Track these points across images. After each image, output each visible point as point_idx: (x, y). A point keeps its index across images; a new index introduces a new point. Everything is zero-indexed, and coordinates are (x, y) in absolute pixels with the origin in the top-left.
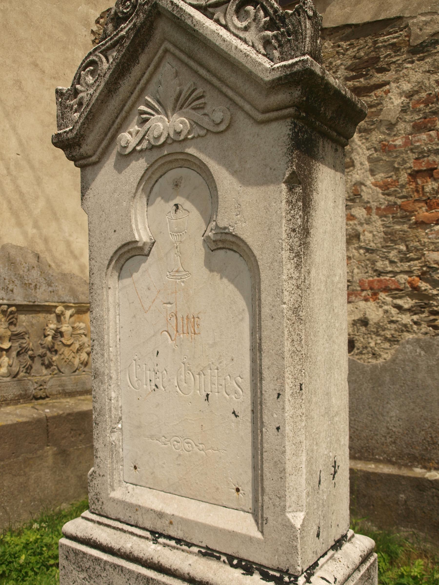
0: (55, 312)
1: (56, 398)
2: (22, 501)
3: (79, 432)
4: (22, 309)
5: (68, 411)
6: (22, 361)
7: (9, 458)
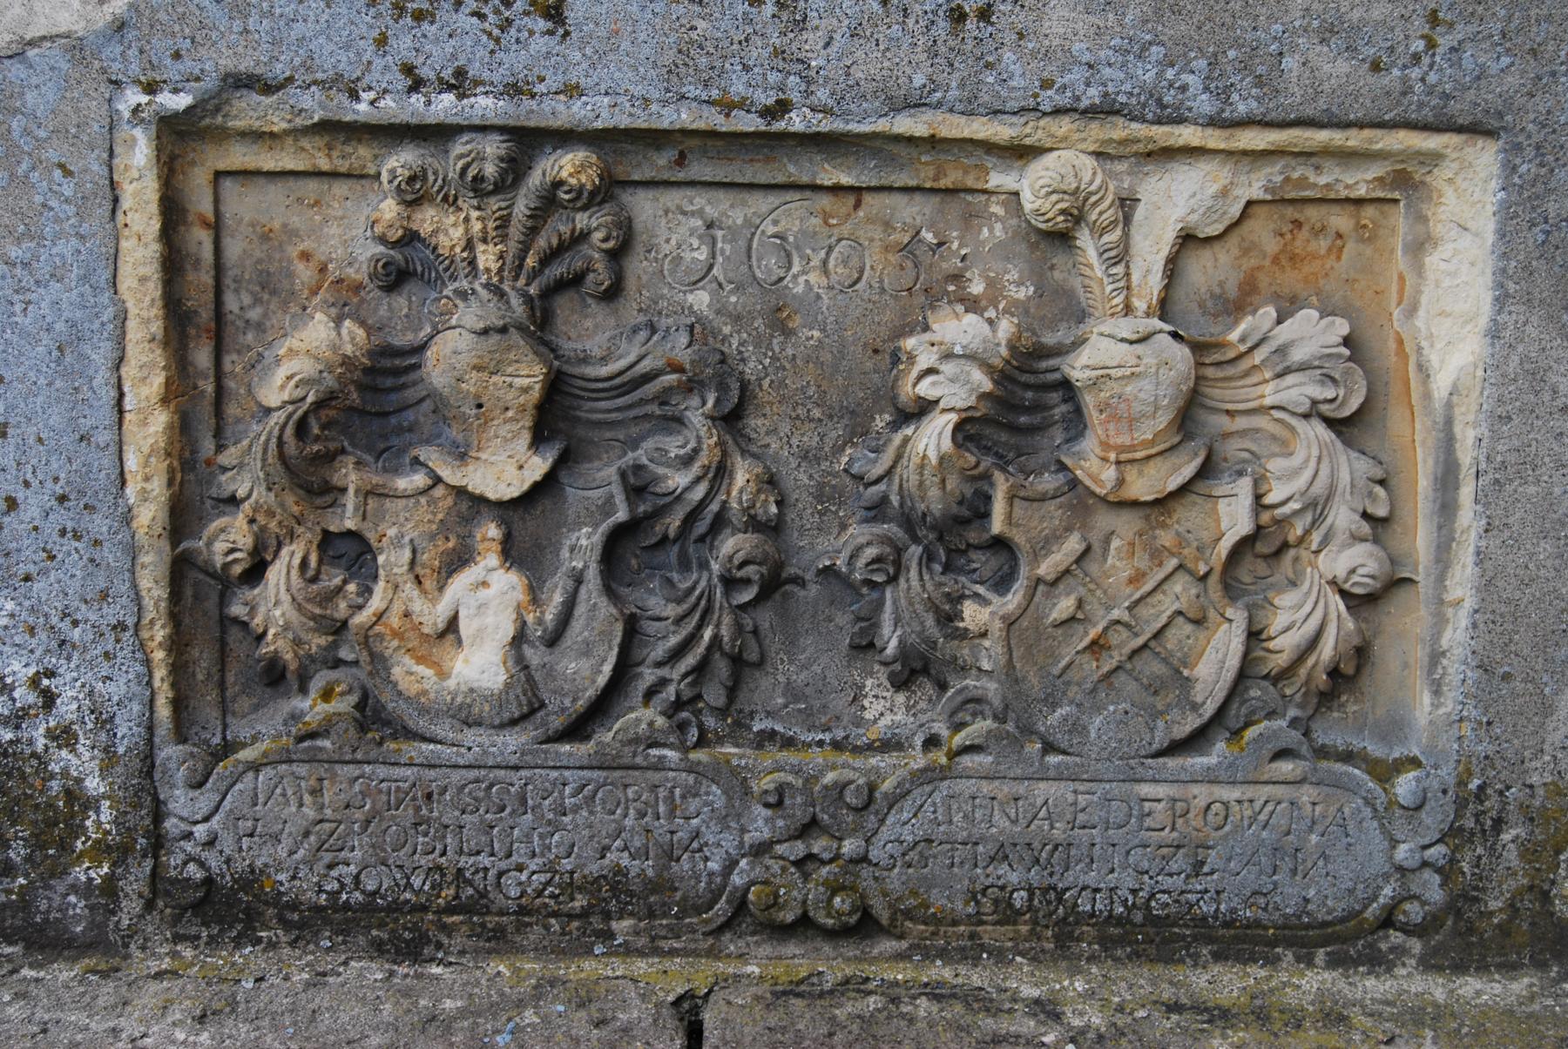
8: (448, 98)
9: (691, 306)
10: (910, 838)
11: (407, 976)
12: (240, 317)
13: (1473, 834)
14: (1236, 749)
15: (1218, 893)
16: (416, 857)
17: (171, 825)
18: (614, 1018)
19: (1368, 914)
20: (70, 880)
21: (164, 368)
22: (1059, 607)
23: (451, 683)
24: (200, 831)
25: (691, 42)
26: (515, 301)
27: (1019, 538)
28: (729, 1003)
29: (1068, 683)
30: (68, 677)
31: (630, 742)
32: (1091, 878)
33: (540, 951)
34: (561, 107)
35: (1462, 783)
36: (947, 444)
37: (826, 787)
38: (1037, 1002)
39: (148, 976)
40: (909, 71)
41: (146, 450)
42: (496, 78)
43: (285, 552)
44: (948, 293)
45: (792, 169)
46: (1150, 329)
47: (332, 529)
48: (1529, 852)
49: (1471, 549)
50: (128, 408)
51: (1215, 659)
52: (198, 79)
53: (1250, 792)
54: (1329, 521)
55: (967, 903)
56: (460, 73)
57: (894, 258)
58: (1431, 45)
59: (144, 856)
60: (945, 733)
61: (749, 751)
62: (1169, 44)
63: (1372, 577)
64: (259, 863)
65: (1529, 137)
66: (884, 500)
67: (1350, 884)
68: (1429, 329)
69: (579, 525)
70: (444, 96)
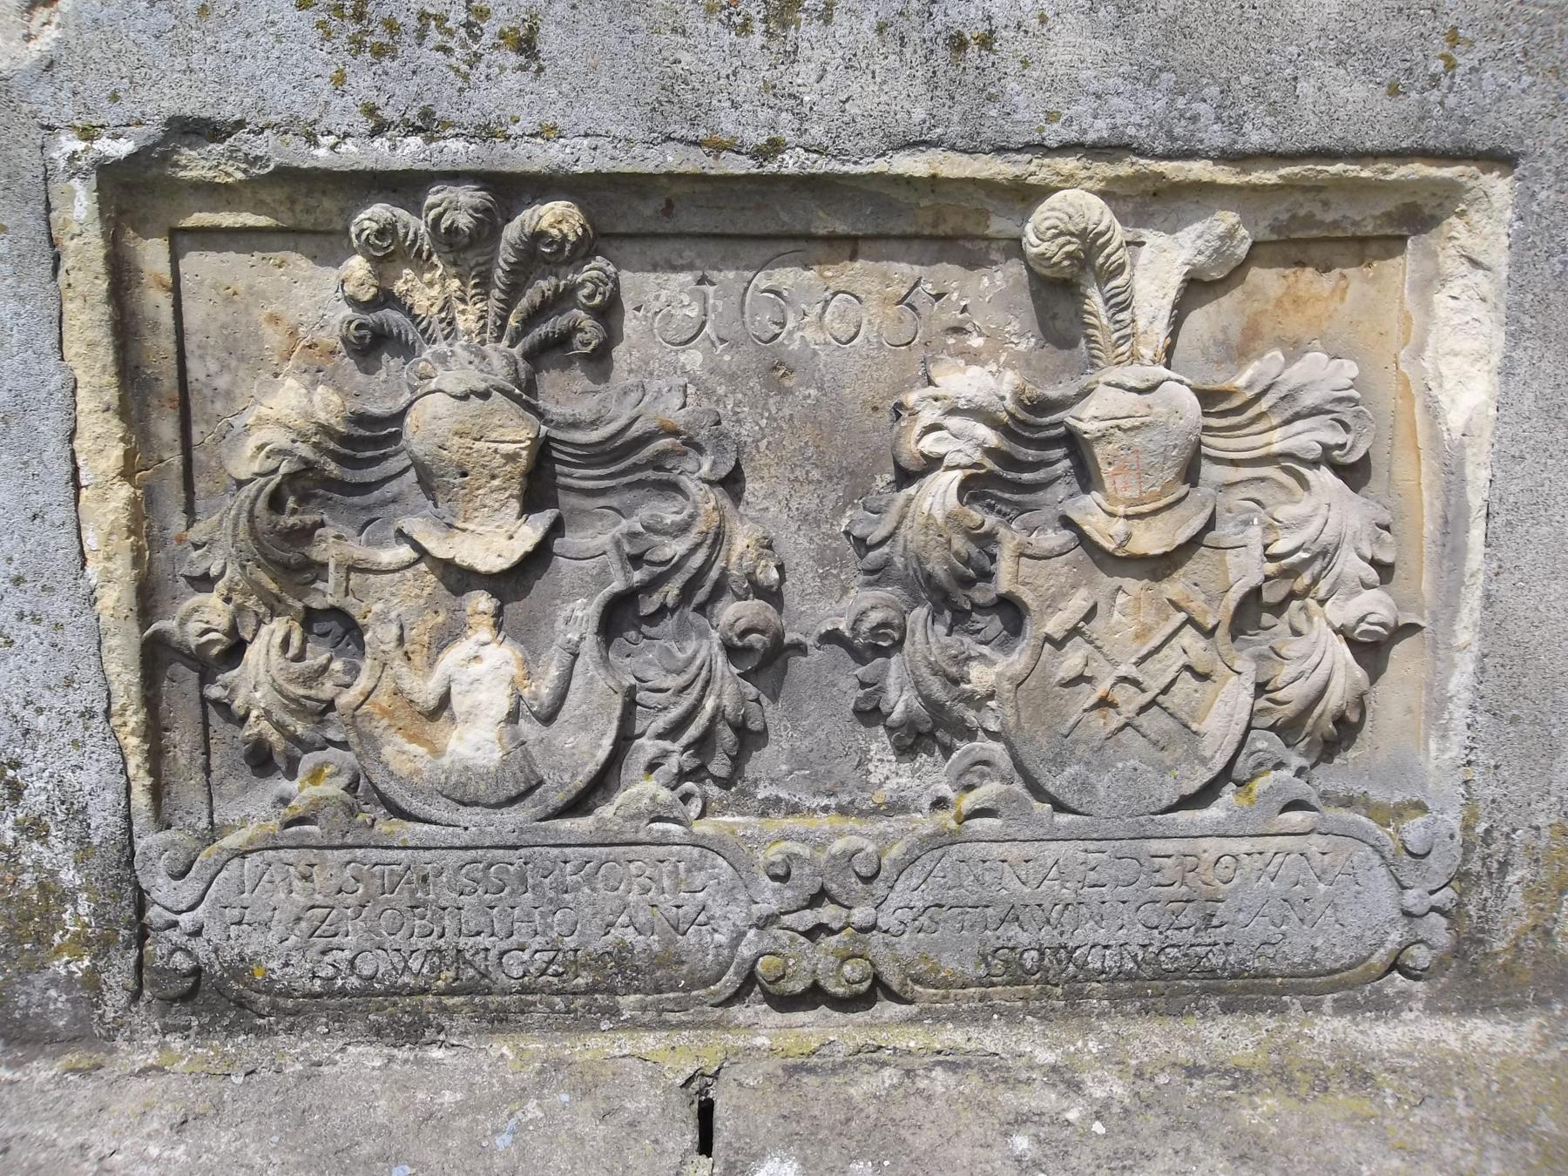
0: (1015, 247)
4: (636, 213)
8: (415, 142)
9: (683, 366)
10: (920, 904)
11: (406, 1061)
12: (207, 386)
13: (1479, 877)
14: (1246, 803)
15: (1227, 944)
16: (413, 940)
17: (154, 914)
18: (622, 1108)
19: (1374, 960)
20: (49, 974)
21: (122, 439)
22: (1065, 665)
23: (446, 761)
24: (185, 920)
25: (675, 77)
26: (497, 362)
27: (1027, 596)
28: (740, 1084)
29: (1076, 742)
30: (35, 767)
31: (632, 817)
32: (1101, 935)
33: (545, 1028)
34: (538, 151)
35: (1467, 827)
36: (952, 500)
37: (834, 857)
38: (1054, 1069)
39: (132, 1074)
40: (907, 106)
41: (106, 527)
42: (465, 118)
43: (264, 630)
44: (947, 347)
45: (785, 217)
46: (1159, 378)
47: (314, 605)
48: (1533, 892)
49: (1479, 593)
50: (84, 483)
51: (1224, 710)
52: (140, 123)
53: (1260, 843)
54: (1337, 570)
55: (977, 965)
56: (426, 114)
57: (893, 311)
58: (1451, 65)
59: (128, 947)
60: (951, 795)
61: (753, 819)
62: (1180, 70)
63: (1382, 625)
64: (248, 951)
65: (1549, 162)
66: (888, 562)
67: (1358, 932)
68: (1437, 369)
69: (571, 596)
70: (410, 140)
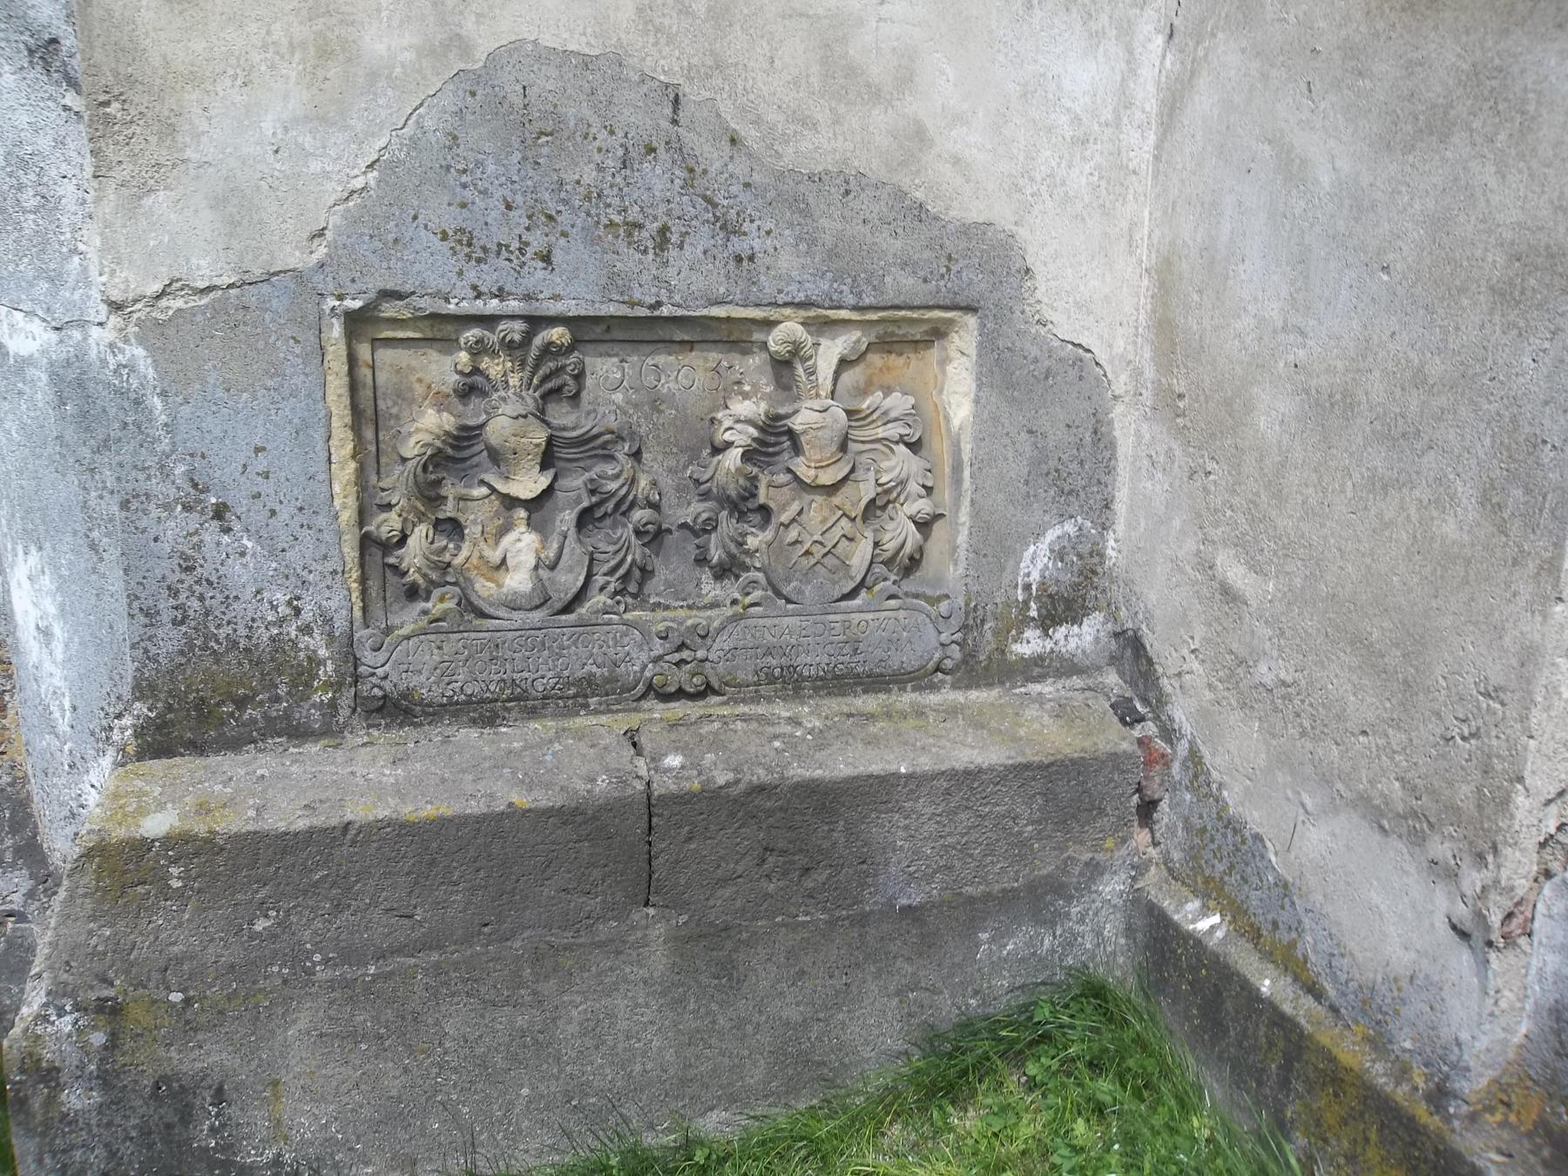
0: (764, 346)
1: (756, 699)
2: (525, 1091)
3: (801, 860)
5: (761, 775)
6: (603, 546)
7: (467, 940)
